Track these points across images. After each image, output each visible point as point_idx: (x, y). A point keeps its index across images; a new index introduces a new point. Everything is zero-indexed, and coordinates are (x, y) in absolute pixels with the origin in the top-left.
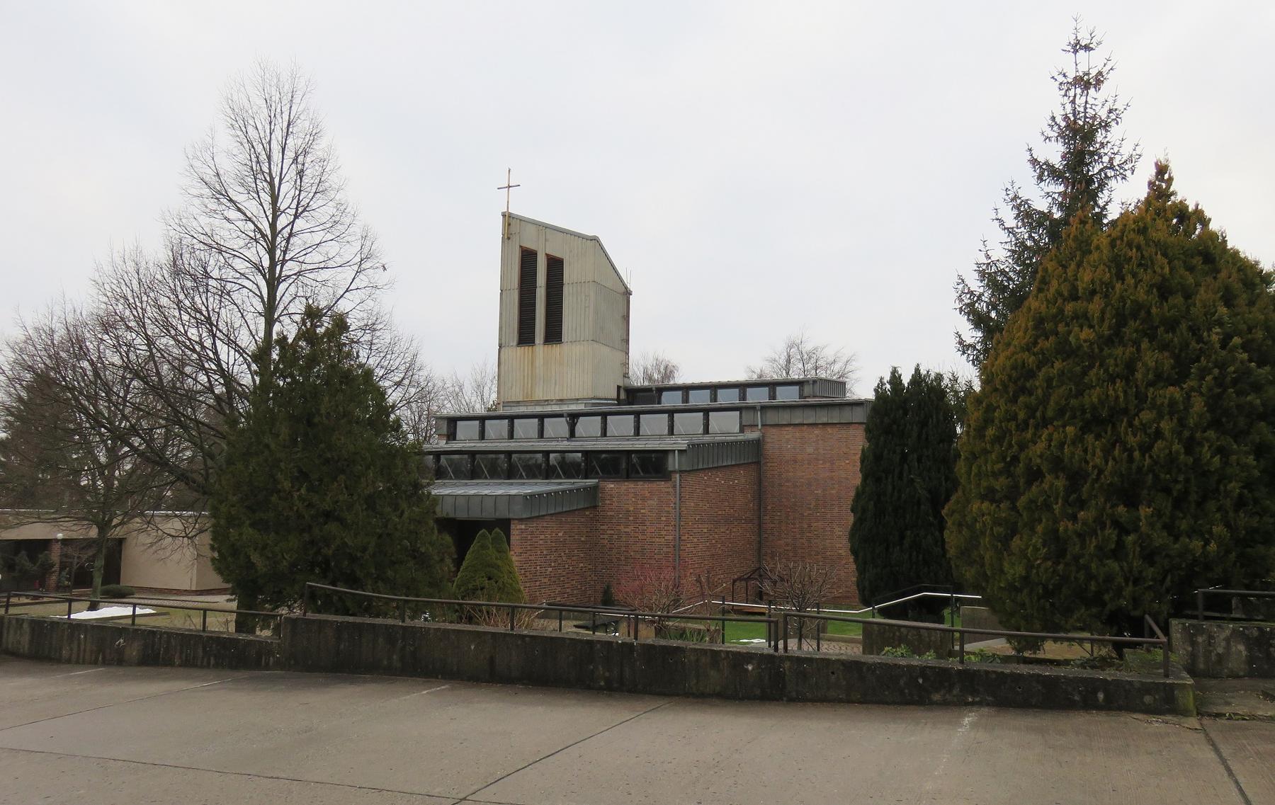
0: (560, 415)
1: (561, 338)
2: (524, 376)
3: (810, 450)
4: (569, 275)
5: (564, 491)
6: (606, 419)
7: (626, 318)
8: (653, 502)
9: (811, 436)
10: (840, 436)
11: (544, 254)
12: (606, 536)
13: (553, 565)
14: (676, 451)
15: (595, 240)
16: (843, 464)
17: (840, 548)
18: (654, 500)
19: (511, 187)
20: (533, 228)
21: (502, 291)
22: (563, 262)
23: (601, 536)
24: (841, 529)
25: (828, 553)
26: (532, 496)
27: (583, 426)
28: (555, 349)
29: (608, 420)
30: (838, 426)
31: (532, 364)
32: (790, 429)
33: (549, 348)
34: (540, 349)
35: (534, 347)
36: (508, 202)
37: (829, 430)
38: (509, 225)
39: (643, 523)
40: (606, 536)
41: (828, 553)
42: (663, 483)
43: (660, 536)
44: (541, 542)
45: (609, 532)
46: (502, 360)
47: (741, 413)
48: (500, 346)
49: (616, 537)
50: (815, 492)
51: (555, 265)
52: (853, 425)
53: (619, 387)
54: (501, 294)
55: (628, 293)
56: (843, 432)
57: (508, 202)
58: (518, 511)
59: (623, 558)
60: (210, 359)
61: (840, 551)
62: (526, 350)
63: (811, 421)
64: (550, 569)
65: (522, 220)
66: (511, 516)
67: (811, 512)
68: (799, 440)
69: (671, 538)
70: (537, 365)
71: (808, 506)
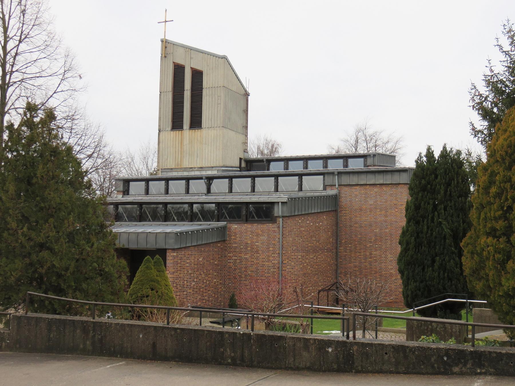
0: (201, 178)
3: (371, 202)
4: (206, 82)
5: (203, 230)
6: (254, 181)
7: (246, 111)
8: (264, 238)
9: (372, 193)
10: (392, 192)
11: (189, 68)
12: (232, 261)
13: (195, 280)
14: (280, 203)
15: (224, 58)
16: (394, 211)
19: (164, 22)
20: (182, 50)
23: (229, 261)
25: (383, 272)
26: (181, 233)
27: (216, 185)
28: (197, 133)
29: (256, 182)
30: (390, 186)
32: (358, 187)
33: (193, 132)
34: (187, 132)
36: (165, 32)
38: (166, 47)
39: (257, 252)
41: (383, 272)
42: (271, 224)
44: (187, 265)
45: (234, 258)
47: (324, 177)
48: (160, 131)
49: (238, 261)
51: (197, 75)
52: (400, 185)
53: (241, 159)
54: (160, 95)
55: (247, 94)
56: (394, 190)
57: (165, 32)
58: (171, 243)
59: (243, 276)
61: (392, 271)
62: (177, 133)
64: (194, 283)
65: (174, 44)
66: (167, 247)
67: (371, 244)
69: (276, 262)
70: (185, 144)
71: (370, 240)
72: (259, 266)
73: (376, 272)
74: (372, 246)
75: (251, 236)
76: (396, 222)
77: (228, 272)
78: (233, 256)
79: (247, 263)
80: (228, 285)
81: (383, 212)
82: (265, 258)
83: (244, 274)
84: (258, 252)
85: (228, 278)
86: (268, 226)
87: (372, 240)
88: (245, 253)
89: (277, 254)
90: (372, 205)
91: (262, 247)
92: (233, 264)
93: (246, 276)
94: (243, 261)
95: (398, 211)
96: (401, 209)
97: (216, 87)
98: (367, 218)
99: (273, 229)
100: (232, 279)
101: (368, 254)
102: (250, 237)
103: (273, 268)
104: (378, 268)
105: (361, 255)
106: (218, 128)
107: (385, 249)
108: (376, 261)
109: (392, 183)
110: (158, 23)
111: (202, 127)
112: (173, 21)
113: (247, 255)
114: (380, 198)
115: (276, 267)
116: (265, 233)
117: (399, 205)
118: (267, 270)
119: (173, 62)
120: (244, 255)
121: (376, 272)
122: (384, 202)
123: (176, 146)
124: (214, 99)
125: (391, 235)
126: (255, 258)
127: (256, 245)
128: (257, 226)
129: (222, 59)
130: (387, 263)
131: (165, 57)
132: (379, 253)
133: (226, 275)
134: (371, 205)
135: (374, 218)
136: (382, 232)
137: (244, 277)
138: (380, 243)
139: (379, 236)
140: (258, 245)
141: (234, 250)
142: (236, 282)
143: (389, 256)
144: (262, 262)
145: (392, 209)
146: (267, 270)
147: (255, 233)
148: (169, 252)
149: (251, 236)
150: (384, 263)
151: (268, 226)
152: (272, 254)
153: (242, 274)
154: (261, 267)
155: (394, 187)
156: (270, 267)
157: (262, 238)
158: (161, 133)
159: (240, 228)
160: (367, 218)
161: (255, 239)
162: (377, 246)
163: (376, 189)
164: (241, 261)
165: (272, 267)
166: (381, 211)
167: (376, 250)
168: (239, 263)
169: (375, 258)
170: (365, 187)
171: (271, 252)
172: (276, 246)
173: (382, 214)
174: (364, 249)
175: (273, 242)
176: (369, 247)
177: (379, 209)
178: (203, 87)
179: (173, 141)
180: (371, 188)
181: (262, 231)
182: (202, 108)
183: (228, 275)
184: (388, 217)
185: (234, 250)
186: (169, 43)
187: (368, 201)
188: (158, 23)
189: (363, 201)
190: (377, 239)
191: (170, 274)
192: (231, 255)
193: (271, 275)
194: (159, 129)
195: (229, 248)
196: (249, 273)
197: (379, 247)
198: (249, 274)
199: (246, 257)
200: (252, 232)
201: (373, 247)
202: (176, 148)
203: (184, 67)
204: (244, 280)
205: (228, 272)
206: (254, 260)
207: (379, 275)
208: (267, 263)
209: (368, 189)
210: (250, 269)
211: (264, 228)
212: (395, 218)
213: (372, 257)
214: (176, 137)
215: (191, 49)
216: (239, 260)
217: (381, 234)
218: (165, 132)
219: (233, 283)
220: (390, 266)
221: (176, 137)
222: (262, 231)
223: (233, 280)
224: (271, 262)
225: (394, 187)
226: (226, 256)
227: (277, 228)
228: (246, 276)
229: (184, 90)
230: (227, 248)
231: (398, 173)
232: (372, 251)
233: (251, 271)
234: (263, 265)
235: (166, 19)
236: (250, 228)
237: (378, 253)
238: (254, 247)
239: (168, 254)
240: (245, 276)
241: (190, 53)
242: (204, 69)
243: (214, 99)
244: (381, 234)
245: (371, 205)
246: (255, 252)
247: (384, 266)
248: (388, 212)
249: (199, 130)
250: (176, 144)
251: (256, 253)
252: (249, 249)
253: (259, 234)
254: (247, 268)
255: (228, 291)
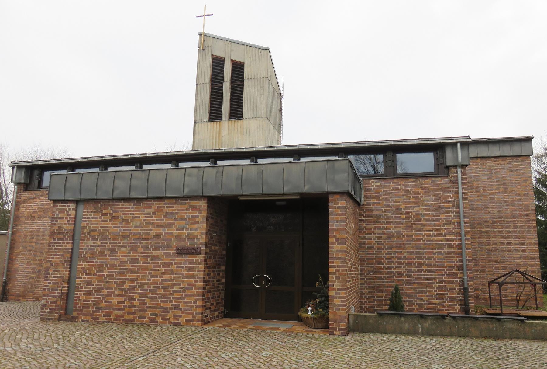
1: (242, 116)
2: (213, 143)
3: (485, 178)
7: (280, 110)
8: (429, 200)
9: (484, 167)
10: (511, 166)
11: (230, 60)
12: (373, 237)
14: (459, 145)
17: (518, 259)
18: (430, 197)
19: (203, 16)
21: (197, 84)
22: (244, 65)
23: (367, 237)
24: (517, 242)
25: (507, 263)
28: (237, 124)
30: (508, 158)
31: (219, 134)
34: (226, 123)
35: (222, 122)
36: (204, 25)
37: (501, 161)
38: (204, 41)
39: (418, 221)
40: (373, 237)
41: (507, 263)
42: (440, 179)
43: (439, 234)
45: (376, 232)
46: (197, 131)
48: (195, 122)
49: (384, 237)
50: (491, 212)
52: (522, 158)
54: (197, 87)
55: (281, 96)
56: (513, 163)
57: (204, 25)
59: (395, 259)
60: (41, 358)
61: (518, 261)
62: (215, 124)
63: (485, 155)
67: (488, 229)
68: (474, 171)
69: (453, 236)
70: (223, 135)
71: (486, 224)
72: (422, 244)
73: (497, 263)
74: (490, 230)
75: (405, 197)
76: (520, 201)
77: (367, 254)
78: (375, 229)
79: (400, 239)
80: (368, 274)
81: (501, 190)
82: (432, 231)
83: (396, 257)
84: (420, 221)
85: (367, 264)
86: (434, 181)
87: (489, 224)
88: (397, 224)
89: (453, 223)
90: (486, 181)
91: (425, 214)
92: (376, 242)
93: (400, 259)
94: (392, 237)
95: (521, 188)
96: (525, 185)
97: (258, 77)
98: (480, 198)
99: (444, 186)
100: (375, 264)
101: (484, 240)
102: (404, 200)
103: (448, 247)
104: (500, 258)
105: (475, 242)
106: (260, 119)
107: (506, 234)
108: (496, 249)
109: (512, 155)
110: (197, 17)
111: (243, 118)
112: (212, 15)
113: (400, 227)
114: (496, 173)
115: (454, 244)
116: (430, 192)
117: (521, 180)
118: (438, 249)
119: (212, 55)
120: (395, 227)
121: (497, 263)
122: (502, 178)
123: (213, 137)
124: (256, 90)
125: (514, 217)
126: (415, 231)
127: (414, 211)
128: (415, 182)
129: (266, 51)
130: (511, 251)
131: (203, 50)
132: (499, 239)
133: (364, 259)
134: (485, 181)
135: (489, 197)
136: (502, 214)
137: (396, 262)
138: (500, 227)
139: (498, 219)
140: (419, 211)
141: (377, 220)
142: (383, 269)
143: (514, 242)
144: (427, 236)
145: (513, 186)
146: (438, 249)
147: (413, 192)
148: (332, 200)
149: (405, 197)
150: (507, 251)
151: (434, 181)
152: (444, 224)
153: (393, 257)
154: (425, 244)
155: (513, 160)
156: (443, 244)
157: (425, 200)
158: (197, 125)
159: (385, 186)
160: (480, 198)
161: (413, 202)
162: (495, 230)
163: (490, 163)
164: (389, 237)
165: (446, 244)
166: (498, 188)
167: (495, 236)
168: (385, 239)
169: (494, 246)
170: (476, 160)
171: (443, 221)
172: (451, 211)
173: (500, 192)
174: (478, 234)
175: (445, 206)
176: (485, 232)
177: (495, 186)
178: (245, 78)
179: (210, 132)
180: (483, 161)
181: (425, 189)
182: (243, 99)
183: (367, 259)
184: (508, 195)
185: (377, 220)
186: (207, 36)
187: (480, 177)
188: (197, 17)
189: (474, 177)
190: (496, 222)
191: (339, 244)
192: (372, 227)
193: (446, 257)
194: (194, 120)
195: (367, 217)
196: (405, 254)
197: (499, 232)
198: (405, 257)
199: (398, 229)
200: (407, 192)
201: (491, 232)
202: (213, 139)
203: (224, 60)
204: (396, 267)
205: (367, 254)
206: (414, 234)
207: (501, 266)
208: (436, 239)
209: (480, 162)
210: (405, 249)
211: (428, 184)
212: (517, 197)
213: (491, 244)
214: (213, 128)
215: (232, 42)
216: (385, 234)
217: (501, 215)
218: (201, 123)
219: (376, 272)
220: (516, 254)
221: (213, 128)
222: (425, 189)
223: (376, 267)
224: (444, 236)
225: (513, 160)
226: (363, 229)
227: (450, 183)
228: (400, 259)
229: (223, 82)
230: (365, 217)
231: (519, 144)
232: (490, 237)
233: (407, 252)
234: (429, 241)
235: (204, 18)
236: (403, 185)
237: (498, 239)
238: (412, 214)
239: (331, 204)
240: (398, 259)
241: (230, 46)
242: (245, 60)
243: (256, 90)
244: (501, 215)
245: (485, 181)
246: (414, 221)
247: (508, 254)
248: (507, 189)
249: (240, 121)
250: (213, 135)
251: (416, 224)
252: (403, 217)
253: (420, 194)
254: (401, 247)
255: (369, 284)
